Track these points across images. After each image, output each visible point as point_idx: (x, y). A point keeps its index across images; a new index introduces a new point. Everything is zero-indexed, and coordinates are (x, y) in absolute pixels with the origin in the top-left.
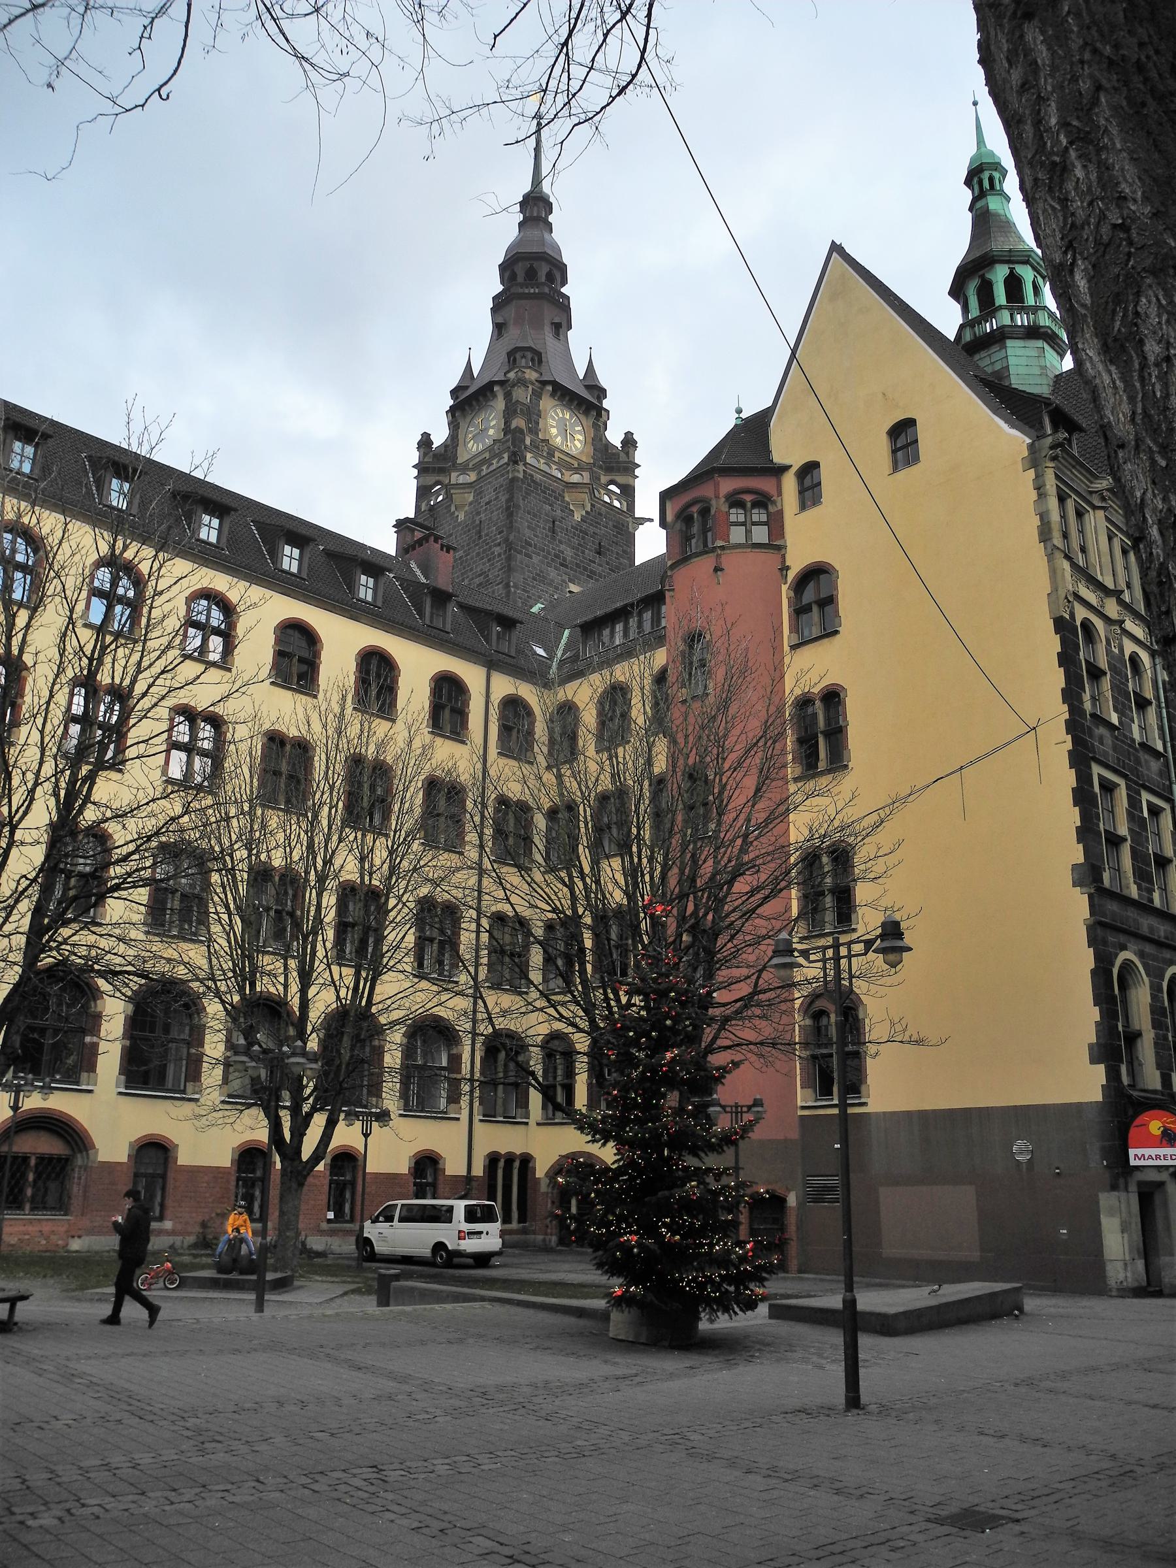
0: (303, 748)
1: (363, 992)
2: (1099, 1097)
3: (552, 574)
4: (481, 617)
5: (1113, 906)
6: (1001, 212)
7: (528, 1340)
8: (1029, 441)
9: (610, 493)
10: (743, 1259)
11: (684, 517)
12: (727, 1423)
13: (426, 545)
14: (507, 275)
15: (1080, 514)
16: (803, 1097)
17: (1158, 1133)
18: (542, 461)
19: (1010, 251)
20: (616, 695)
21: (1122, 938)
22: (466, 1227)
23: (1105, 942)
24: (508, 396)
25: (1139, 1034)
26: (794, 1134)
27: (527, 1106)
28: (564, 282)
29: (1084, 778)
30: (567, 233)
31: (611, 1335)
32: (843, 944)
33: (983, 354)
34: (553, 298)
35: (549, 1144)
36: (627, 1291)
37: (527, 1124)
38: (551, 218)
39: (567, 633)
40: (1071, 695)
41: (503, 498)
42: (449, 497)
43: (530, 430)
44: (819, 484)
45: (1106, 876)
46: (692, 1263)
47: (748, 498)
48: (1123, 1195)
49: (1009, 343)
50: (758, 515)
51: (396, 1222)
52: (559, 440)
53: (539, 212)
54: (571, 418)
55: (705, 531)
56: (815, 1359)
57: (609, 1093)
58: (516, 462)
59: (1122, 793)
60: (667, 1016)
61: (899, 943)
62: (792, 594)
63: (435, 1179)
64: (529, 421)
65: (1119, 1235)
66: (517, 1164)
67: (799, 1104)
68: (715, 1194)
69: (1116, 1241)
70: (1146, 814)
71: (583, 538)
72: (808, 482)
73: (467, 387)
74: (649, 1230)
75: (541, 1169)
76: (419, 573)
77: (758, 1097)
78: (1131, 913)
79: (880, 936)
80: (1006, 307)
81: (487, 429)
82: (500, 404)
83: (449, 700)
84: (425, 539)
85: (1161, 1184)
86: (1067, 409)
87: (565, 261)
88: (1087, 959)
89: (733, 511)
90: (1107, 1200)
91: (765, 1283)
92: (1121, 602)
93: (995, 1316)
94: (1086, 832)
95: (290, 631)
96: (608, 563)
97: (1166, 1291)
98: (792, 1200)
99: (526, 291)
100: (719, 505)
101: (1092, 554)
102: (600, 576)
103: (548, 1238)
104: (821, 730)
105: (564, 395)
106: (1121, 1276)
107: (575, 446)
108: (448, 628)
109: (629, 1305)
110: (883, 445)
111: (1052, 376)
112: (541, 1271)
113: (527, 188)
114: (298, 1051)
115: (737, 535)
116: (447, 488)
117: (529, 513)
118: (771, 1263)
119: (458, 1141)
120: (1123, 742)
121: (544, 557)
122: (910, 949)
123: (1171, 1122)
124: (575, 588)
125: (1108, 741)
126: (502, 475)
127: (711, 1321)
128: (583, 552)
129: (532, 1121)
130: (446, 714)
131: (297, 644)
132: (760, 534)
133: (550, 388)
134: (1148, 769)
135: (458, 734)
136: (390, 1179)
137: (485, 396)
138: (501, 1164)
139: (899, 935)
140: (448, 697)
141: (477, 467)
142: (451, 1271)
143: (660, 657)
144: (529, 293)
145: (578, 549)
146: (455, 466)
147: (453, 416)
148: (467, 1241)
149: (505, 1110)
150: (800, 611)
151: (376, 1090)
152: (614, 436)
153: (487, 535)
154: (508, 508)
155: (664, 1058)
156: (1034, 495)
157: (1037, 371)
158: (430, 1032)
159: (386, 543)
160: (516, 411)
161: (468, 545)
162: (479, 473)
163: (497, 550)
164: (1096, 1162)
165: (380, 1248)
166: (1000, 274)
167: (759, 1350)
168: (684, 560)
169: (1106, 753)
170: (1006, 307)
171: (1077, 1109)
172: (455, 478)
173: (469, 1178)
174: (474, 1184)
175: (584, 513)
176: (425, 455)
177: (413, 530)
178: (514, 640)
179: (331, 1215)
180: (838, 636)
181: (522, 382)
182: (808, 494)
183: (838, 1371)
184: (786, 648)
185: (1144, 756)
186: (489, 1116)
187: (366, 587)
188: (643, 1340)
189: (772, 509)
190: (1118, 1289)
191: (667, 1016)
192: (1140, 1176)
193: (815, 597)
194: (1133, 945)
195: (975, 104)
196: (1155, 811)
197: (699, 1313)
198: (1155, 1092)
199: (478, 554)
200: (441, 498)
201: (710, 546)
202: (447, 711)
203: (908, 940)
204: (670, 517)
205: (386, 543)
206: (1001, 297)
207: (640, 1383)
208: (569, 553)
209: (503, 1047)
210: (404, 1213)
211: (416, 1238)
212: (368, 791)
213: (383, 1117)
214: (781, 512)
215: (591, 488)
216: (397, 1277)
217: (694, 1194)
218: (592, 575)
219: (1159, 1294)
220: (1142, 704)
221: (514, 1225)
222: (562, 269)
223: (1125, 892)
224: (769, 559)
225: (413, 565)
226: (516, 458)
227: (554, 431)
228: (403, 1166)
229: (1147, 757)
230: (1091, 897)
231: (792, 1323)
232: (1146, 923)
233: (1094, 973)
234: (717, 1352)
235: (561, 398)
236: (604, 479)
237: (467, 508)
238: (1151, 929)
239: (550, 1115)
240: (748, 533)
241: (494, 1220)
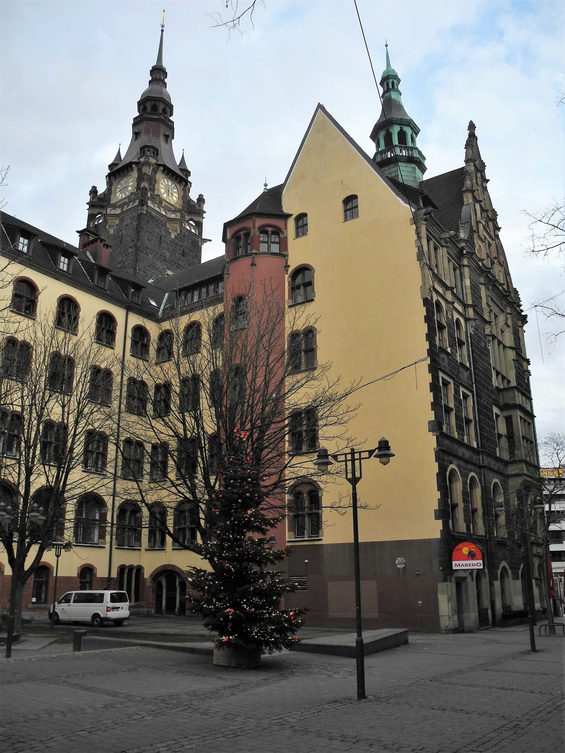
0: (26, 347)
1: (61, 479)
2: (438, 536)
3: (159, 264)
4: (124, 284)
5: (447, 442)
6: (397, 100)
8: (413, 210)
9: (190, 225)
11: (237, 237)
12: (303, 711)
13: (95, 244)
14: (141, 108)
15: (436, 249)
17: (467, 553)
18: (156, 206)
19: (401, 119)
20: (194, 329)
21: (451, 458)
22: (111, 605)
23: (443, 460)
24: (140, 170)
25: (457, 505)
28: (171, 114)
29: (435, 378)
30: (174, 89)
31: (214, 663)
32: (357, 453)
33: (386, 168)
34: (166, 122)
37: (140, 550)
38: (166, 80)
39: (167, 294)
40: (430, 337)
41: (135, 223)
42: (105, 221)
43: (150, 189)
44: (307, 224)
45: (444, 427)
47: (270, 229)
48: (449, 583)
49: (400, 164)
50: (275, 238)
51: (72, 603)
52: (165, 196)
53: (160, 76)
54: (172, 185)
55: (246, 244)
56: (325, 672)
57: (215, 532)
58: (143, 205)
59: (452, 386)
60: (248, 491)
62: (290, 279)
64: (150, 184)
65: (447, 603)
66: (134, 571)
67: (287, 539)
69: (445, 607)
70: (462, 398)
71: (175, 247)
72: (300, 223)
73: (117, 164)
74: (236, 606)
75: (147, 574)
76: (91, 258)
77: (273, 535)
78: (455, 446)
79: (378, 448)
80: (398, 146)
81: (127, 187)
82: (135, 174)
83: (106, 326)
84: (94, 241)
85: (465, 578)
86: (430, 196)
87: (173, 103)
88: (435, 468)
89: (262, 235)
90: (441, 586)
91: (295, 633)
92: (453, 293)
93: (397, 645)
94: (436, 405)
95: (22, 284)
96: (187, 261)
97: (466, 630)
99: (152, 117)
100: (255, 232)
101: (440, 268)
102: (183, 267)
103: (150, 610)
104: (303, 350)
105: (169, 172)
106: (447, 624)
107: (173, 199)
108: (107, 288)
110: (340, 207)
111: (418, 182)
113: (154, 63)
114: (35, 509)
115: (263, 248)
116: (105, 216)
117: (148, 232)
119: (102, 559)
120: (453, 362)
121: (155, 255)
122: (393, 455)
123: (474, 548)
124: (170, 273)
125: (446, 361)
126: (135, 211)
127: (270, 653)
128: (175, 254)
131: (24, 290)
132: (275, 248)
133: (162, 168)
134: (463, 375)
135: (110, 344)
137: (127, 169)
138: (126, 571)
139: (388, 448)
140: (106, 325)
141: (122, 206)
142: (102, 629)
143: (220, 308)
144: (153, 118)
145: (172, 253)
146: (109, 205)
147: (110, 178)
148: (111, 612)
149: (129, 543)
150: (294, 289)
151: (61, 531)
152: (193, 196)
153: (125, 242)
154: (137, 229)
155: (247, 513)
156: (415, 237)
157: (412, 179)
158: (91, 501)
159: (74, 241)
160: (143, 178)
161: (115, 246)
162: (122, 210)
163: (130, 250)
164: (437, 568)
165: (62, 617)
166: (395, 130)
167: (294, 668)
168: (235, 259)
169: (445, 367)
170: (398, 146)
171: (429, 541)
172: (109, 211)
173: (109, 579)
174: (112, 582)
175: (176, 234)
176: (93, 198)
177: (88, 235)
178: (140, 296)
179: (34, 600)
180: (313, 302)
181: (147, 164)
182: (300, 230)
183: (353, 680)
184: (286, 306)
185: (461, 370)
186: (121, 545)
187: (63, 264)
189: (281, 236)
190: (446, 630)
191: (248, 491)
192: (457, 575)
193: (302, 281)
194: (455, 461)
195: (386, 46)
196: (465, 397)
198: (463, 533)
199: (120, 252)
200: (101, 221)
201: (249, 251)
202: (105, 332)
204: (228, 236)
205: (74, 241)
206: (396, 141)
207: (243, 690)
208: (168, 254)
210: (77, 598)
211: (82, 611)
212: (60, 372)
214: (286, 238)
215: (181, 221)
216: (84, 634)
218: (179, 266)
219: (463, 631)
220: (461, 344)
221: (133, 603)
222: (171, 107)
223: (452, 435)
224: (278, 261)
225: (88, 254)
226: (143, 203)
227: (163, 191)
228: (74, 573)
229: (463, 370)
230: (437, 437)
231: (303, 653)
232: (461, 451)
233: (438, 474)
234: (273, 670)
235: (167, 174)
236: (187, 218)
237: (115, 227)
238: (463, 454)
239: (152, 545)
240: (269, 247)
241: (126, 601)
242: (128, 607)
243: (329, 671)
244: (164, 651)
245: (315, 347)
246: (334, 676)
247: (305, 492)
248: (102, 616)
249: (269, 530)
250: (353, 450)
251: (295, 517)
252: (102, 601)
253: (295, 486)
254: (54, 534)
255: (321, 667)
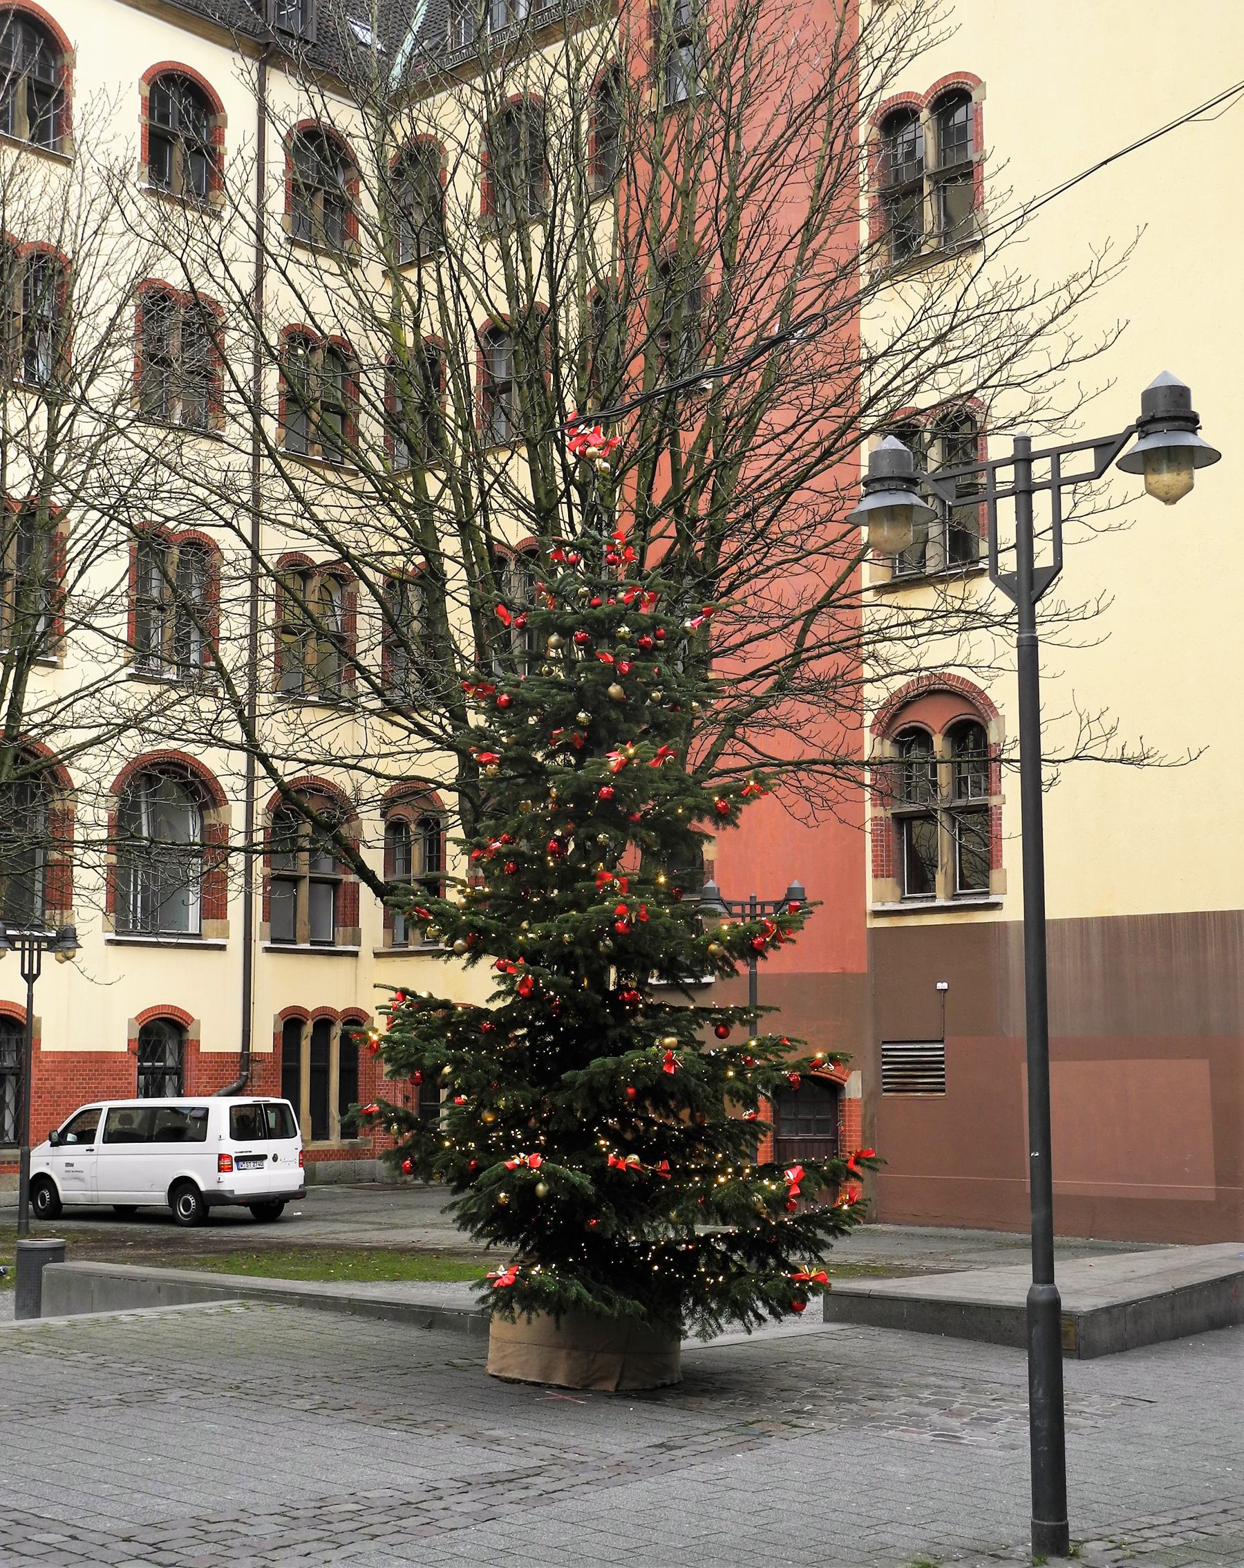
7: (306, 1387)
10: (779, 1203)
16: (877, 894)
26: (859, 963)
27: (355, 922)
31: (491, 1369)
32: (1043, 454)
35: (363, 981)
36: (524, 1275)
37: (355, 954)
46: (666, 1216)
56: (935, 1416)
60: (612, 675)
61: (1188, 440)
63: (181, 1061)
67: (871, 906)
68: (717, 1063)
77: (796, 884)
98: (854, 1087)
109: (528, 1307)
112: (380, 1227)
118: (836, 1212)
119: (224, 988)
122: (1211, 456)
129: (365, 950)
130: (177, 155)
136: (90, 1067)
138: (308, 1029)
139: (1191, 422)
149: (313, 931)
151: (61, 896)
165: (68, 1192)
167: (812, 1397)
173: (246, 1058)
174: (256, 1068)
186: (282, 943)
188: (559, 1380)
191: (612, 675)
197: (681, 1321)
203: (1206, 437)
209: (307, 818)
210: (115, 1125)
211: (135, 1172)
213: (65, 942)
216: (57, 1254)
217: (671, 1062)
221: (334, 1141)
228: (116, 1038)
231: (876, 1331)
242: (296, 1156)
243: (951, 1414)
244: (324, 1320)
245: (975, 158)
246: (967, 1436)
247: (937, 730)
248: (203, 1188)
249: (709, 838)
250: (1023, 442)
251: (901, 820)
252: (201, 1137)
253: (903, 703)
254: (38, 903)
255: (925, 1394)
